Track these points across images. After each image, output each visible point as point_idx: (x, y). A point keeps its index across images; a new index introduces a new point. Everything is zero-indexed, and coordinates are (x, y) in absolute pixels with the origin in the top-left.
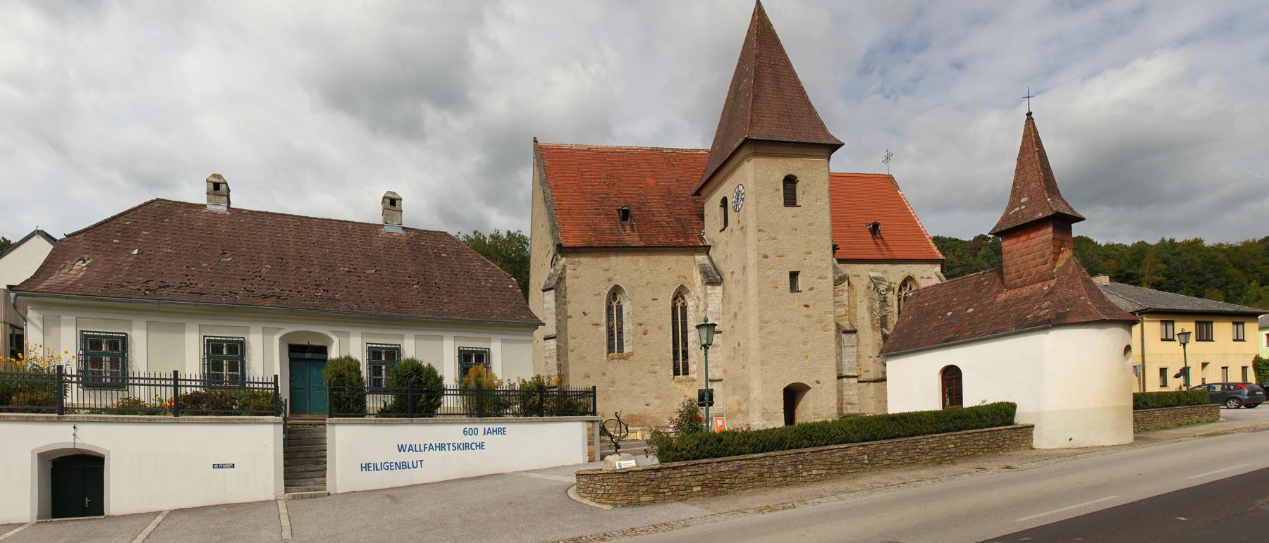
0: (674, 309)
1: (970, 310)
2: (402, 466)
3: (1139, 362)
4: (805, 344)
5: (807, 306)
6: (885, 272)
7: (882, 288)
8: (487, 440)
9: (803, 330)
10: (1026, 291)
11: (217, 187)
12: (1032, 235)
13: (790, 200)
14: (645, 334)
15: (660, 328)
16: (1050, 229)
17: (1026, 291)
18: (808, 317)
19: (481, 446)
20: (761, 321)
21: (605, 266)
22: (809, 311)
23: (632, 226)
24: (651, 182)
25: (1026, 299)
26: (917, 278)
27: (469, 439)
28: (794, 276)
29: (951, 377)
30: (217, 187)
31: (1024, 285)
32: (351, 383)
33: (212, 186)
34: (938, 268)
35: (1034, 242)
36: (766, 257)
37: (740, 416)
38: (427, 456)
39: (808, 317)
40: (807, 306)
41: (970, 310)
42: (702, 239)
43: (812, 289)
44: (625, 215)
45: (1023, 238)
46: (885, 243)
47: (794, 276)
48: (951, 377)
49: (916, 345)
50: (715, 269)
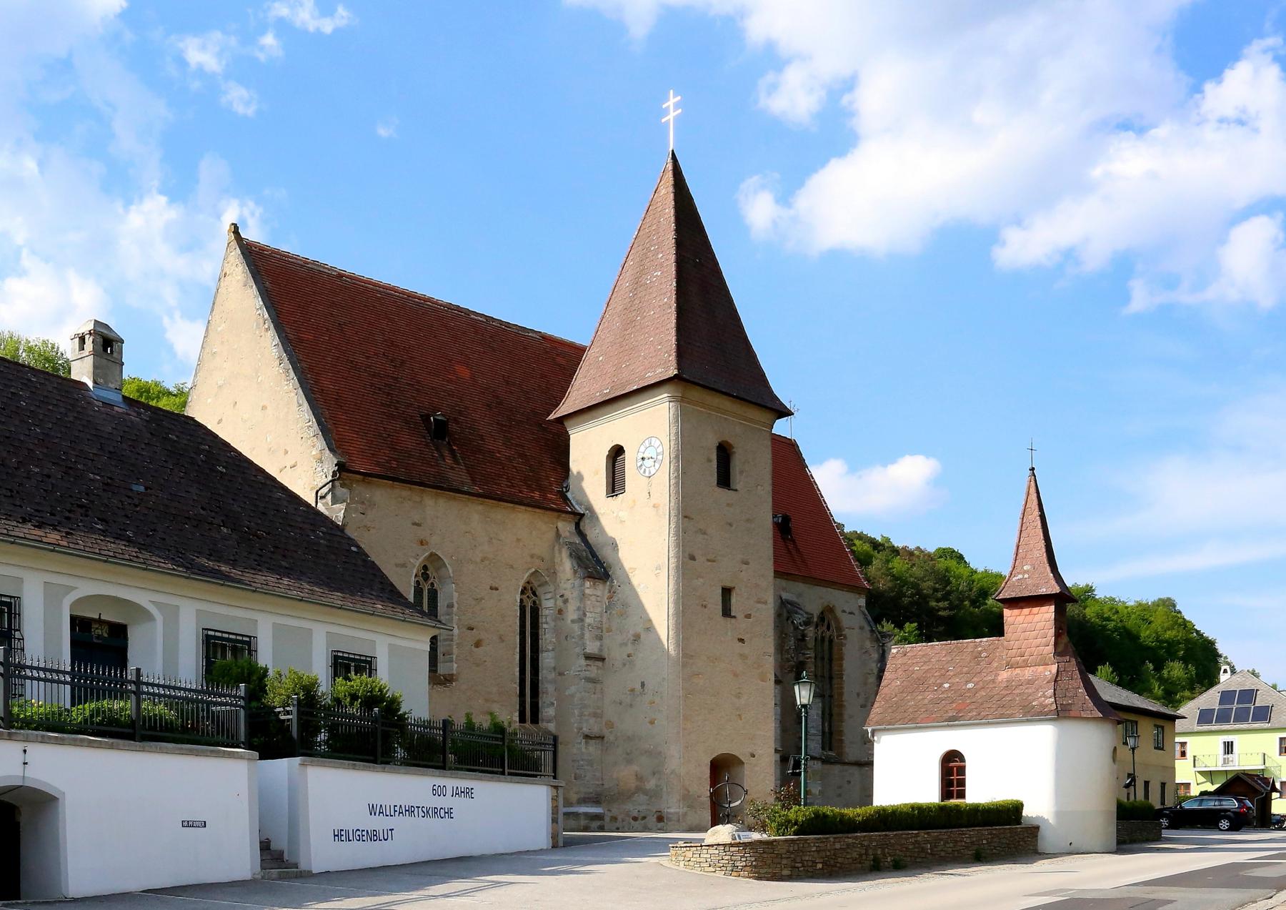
0: (522, 608)
1: (970, 686)
4: (738, 696)
5: (741, 640)
6: (800, 595)
7: (798, 619)
9: (736, 675)
11: (106, 344)
12: (1035, 610)
13: (724, 480)
14: (478, 644)
16: (1053, 608)
21: (417, 518)
22: (745, 649)
23: (452, 452)
24: (464, 373)
25: (1030, 682)
28: (727, 592)
29: (952, 769)
30: (106, 344)
31: (1026, 665)
32: (1218, 792)
34: (862, 602)
35: (1037, 618)
37: (642, 798)
39: (743, 657)
40: (741, 640)
41: (970, 686)
42: (566, 499)
43: (748, 616)
45: (1026, 611)
46: (798, 550)
47: (727, 592)
48: (952, 769)
49: (912, 720)
50: (594, 554)
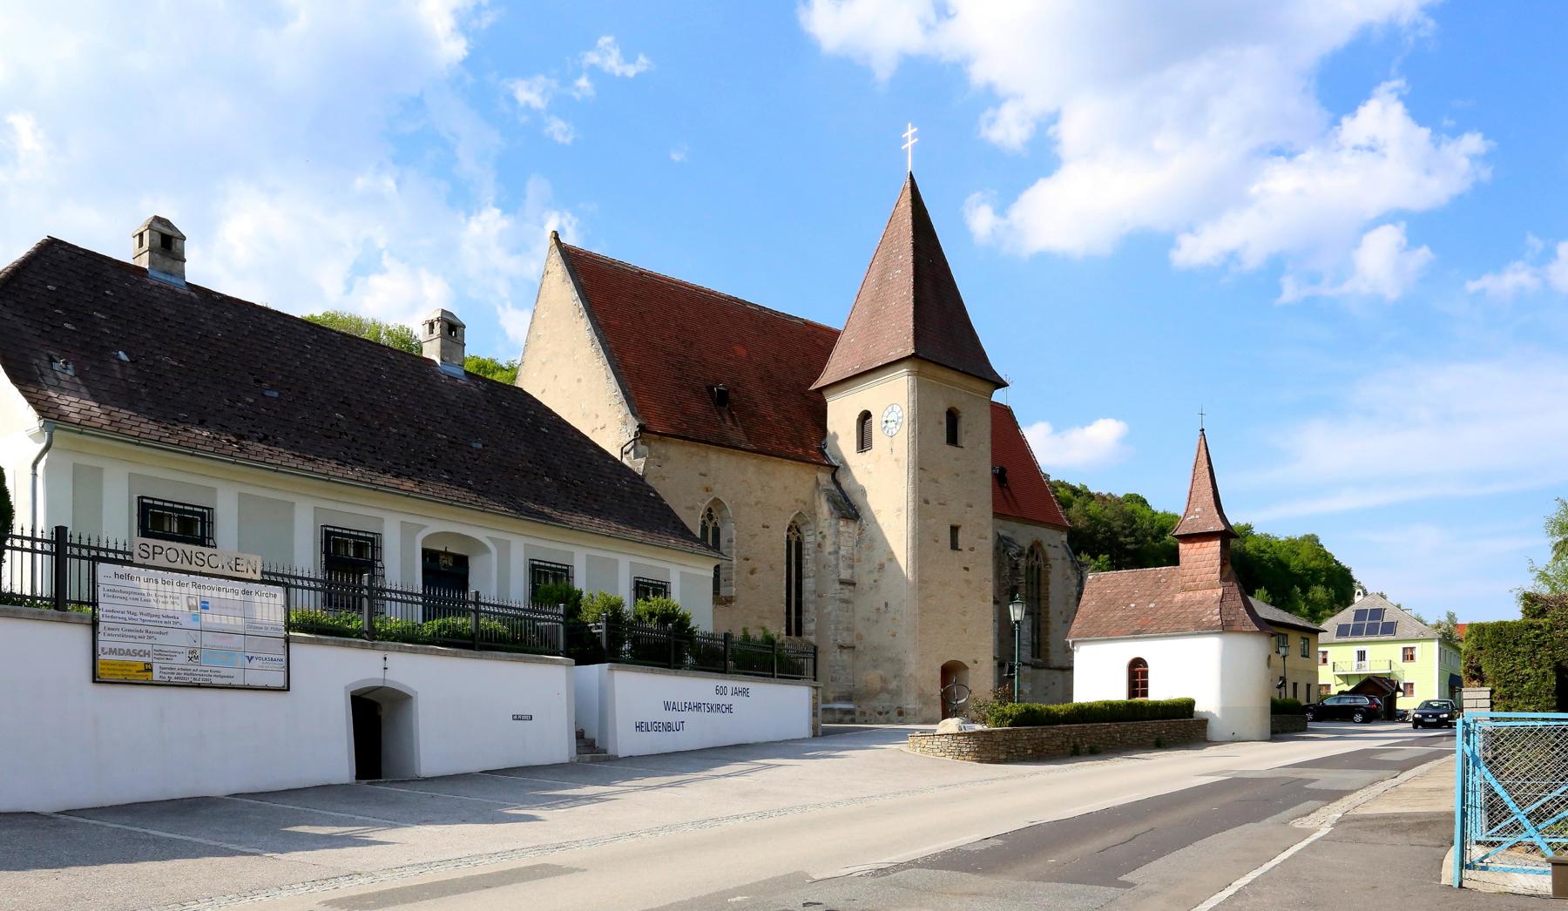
2: (668, 727)
3: (137, 560)
4: (964, 613)
8: (736, 701)
10: (1199, 595)
13: (953, 439)
14: (752, 572)
15: (771, 567)
17: (1199, 595)
18: (968, 582)
19: (729, 708)
20: (921, 581)
21: (703, 470)
23: (732, 416)
24: (742, 352)
25: (1200, 603)
26: (1045, 546)
27: (721, 700)
28: (954, 530)
29: (1137, 672)
31: (1197, 589)
33: (158, 241)
34: (1064, 537)
36: (927, 502)
37: (886, 696)
38: (687, 716)
39: (968, 582)
43: (972, 549)
44: (722, 399)
45: (1197, 545)
47: (954, 530)
48: (1137, 672)
49: (1105, 633)
50: (847, 499)
